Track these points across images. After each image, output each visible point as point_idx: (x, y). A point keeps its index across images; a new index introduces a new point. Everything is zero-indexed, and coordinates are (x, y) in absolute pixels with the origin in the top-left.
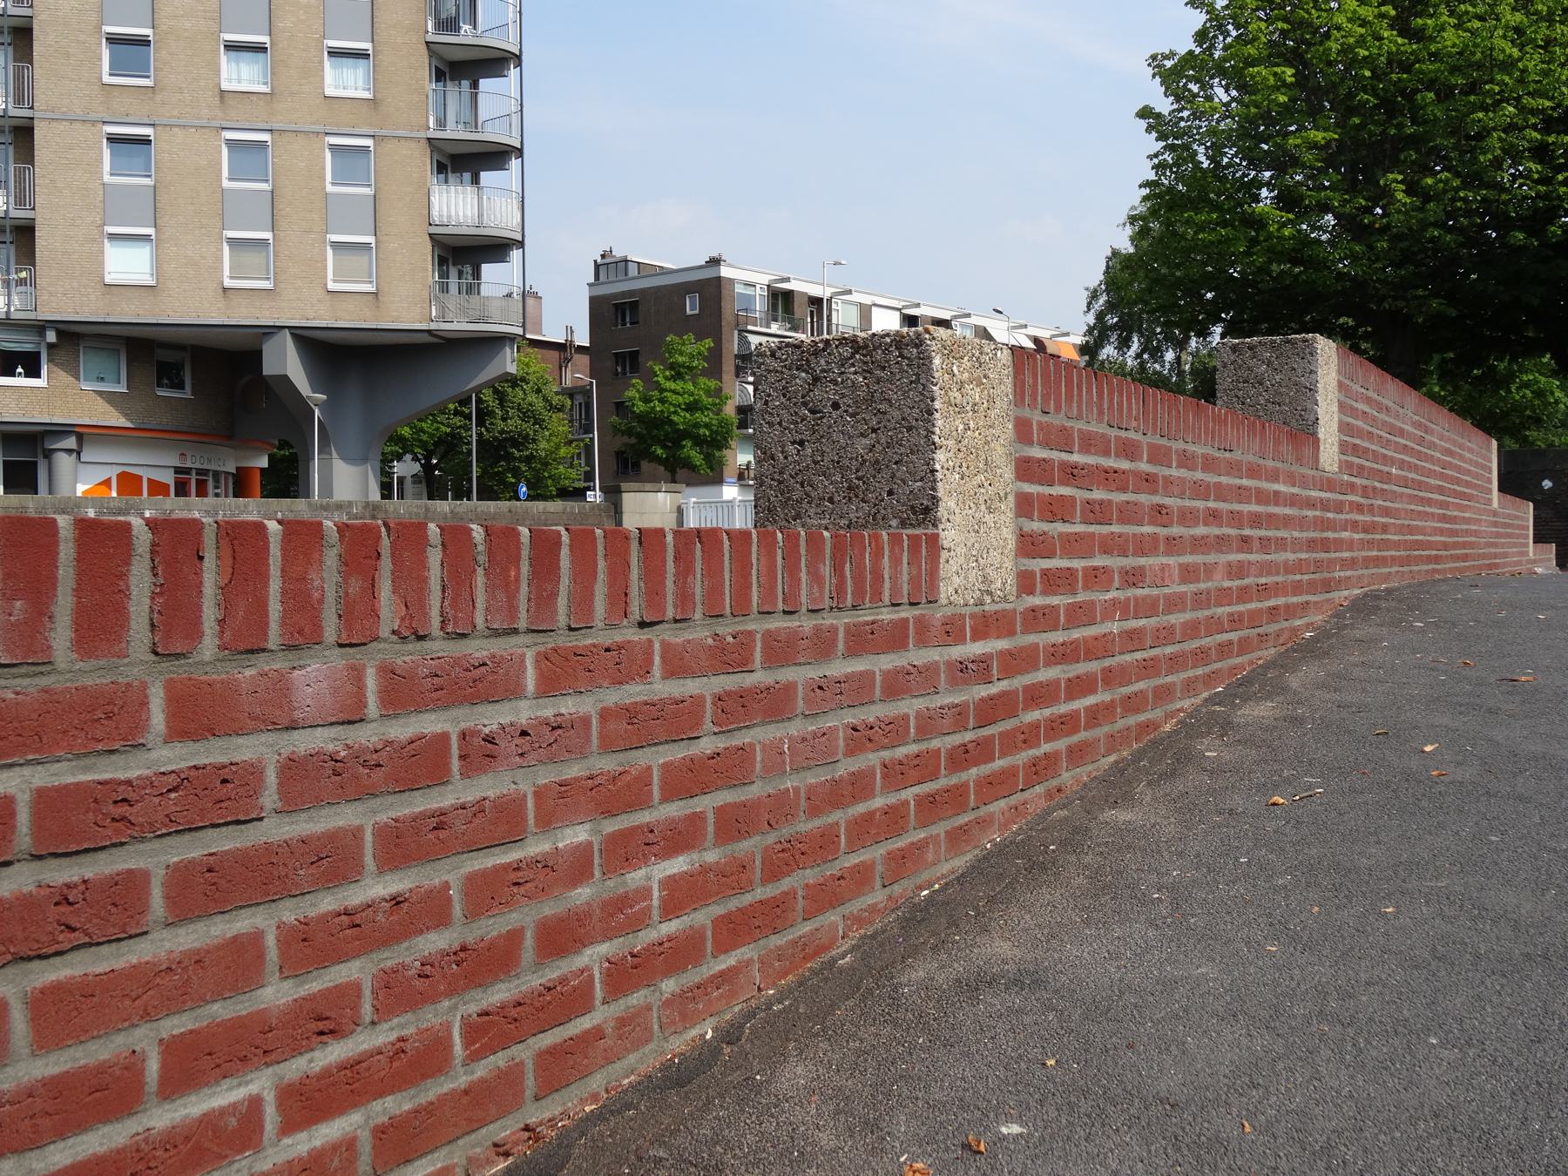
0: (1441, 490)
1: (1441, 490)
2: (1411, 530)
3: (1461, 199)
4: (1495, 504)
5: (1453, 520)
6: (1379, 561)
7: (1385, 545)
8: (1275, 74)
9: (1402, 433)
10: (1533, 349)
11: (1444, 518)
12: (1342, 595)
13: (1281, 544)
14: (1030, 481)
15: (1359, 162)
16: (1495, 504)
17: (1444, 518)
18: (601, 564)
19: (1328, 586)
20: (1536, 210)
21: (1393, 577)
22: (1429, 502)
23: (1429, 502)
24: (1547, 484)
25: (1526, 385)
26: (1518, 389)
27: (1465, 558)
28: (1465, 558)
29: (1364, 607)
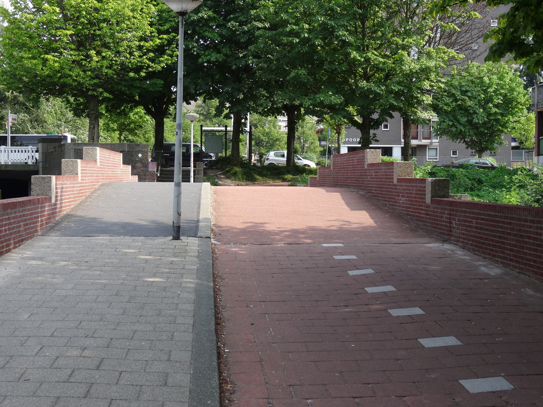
0: (112, 166)
1: (112, 166)
2: (107, 174)
3: (114, 61)
4: (122, 167)
5: (114, 171)
6: (103, 179)
7: (104, 176)
8: (53, 9)
9: (106, 158)
10: (137, 104)
11: (112, 171)
12: (100, 184)
13: (93, 176)
14: (189, 178)
15: (82, 42)
16: (122, 167)
17: (112, 171)
18: (169, 169)
19: (98, 182)
20: (137, 66)
21: (105, 181)
22: (110, 168)
23: (110, 168)
24: (140, 155)
25: (137, 113)
26: (133, 115)
27: (116, 179)
28: (116, 179)
29: (102, 185)
